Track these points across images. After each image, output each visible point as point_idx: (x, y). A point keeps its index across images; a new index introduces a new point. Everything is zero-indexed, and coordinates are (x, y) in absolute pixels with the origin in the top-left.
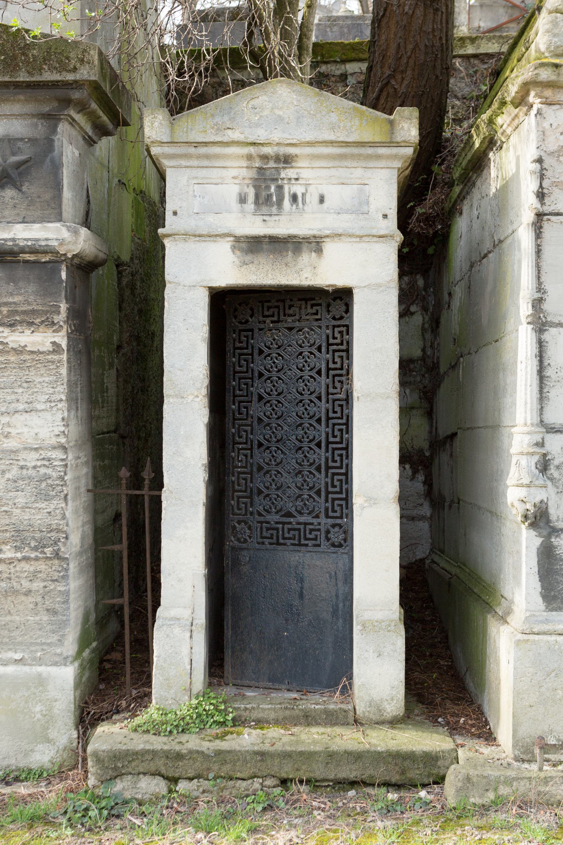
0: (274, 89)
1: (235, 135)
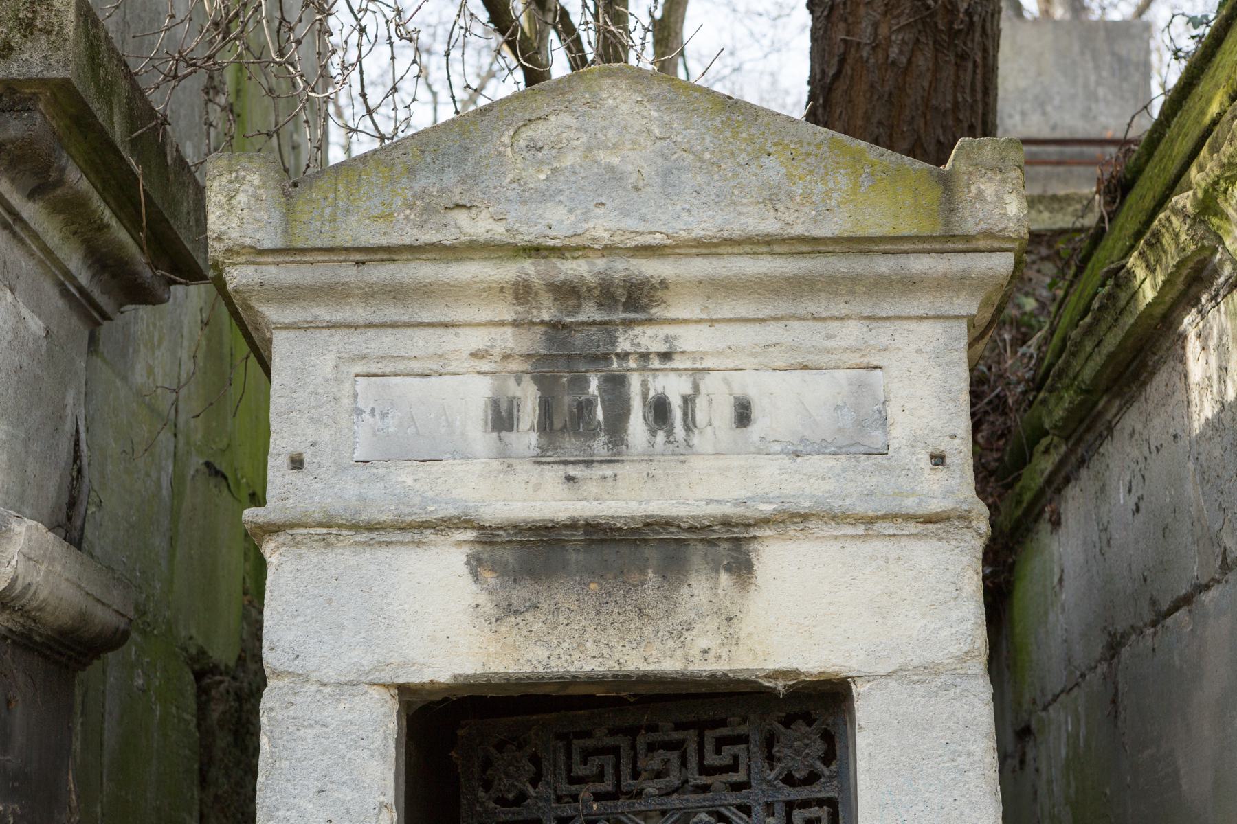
0: (594, 95)
1: (477, 226)
